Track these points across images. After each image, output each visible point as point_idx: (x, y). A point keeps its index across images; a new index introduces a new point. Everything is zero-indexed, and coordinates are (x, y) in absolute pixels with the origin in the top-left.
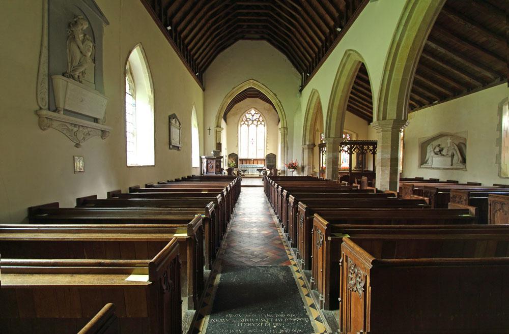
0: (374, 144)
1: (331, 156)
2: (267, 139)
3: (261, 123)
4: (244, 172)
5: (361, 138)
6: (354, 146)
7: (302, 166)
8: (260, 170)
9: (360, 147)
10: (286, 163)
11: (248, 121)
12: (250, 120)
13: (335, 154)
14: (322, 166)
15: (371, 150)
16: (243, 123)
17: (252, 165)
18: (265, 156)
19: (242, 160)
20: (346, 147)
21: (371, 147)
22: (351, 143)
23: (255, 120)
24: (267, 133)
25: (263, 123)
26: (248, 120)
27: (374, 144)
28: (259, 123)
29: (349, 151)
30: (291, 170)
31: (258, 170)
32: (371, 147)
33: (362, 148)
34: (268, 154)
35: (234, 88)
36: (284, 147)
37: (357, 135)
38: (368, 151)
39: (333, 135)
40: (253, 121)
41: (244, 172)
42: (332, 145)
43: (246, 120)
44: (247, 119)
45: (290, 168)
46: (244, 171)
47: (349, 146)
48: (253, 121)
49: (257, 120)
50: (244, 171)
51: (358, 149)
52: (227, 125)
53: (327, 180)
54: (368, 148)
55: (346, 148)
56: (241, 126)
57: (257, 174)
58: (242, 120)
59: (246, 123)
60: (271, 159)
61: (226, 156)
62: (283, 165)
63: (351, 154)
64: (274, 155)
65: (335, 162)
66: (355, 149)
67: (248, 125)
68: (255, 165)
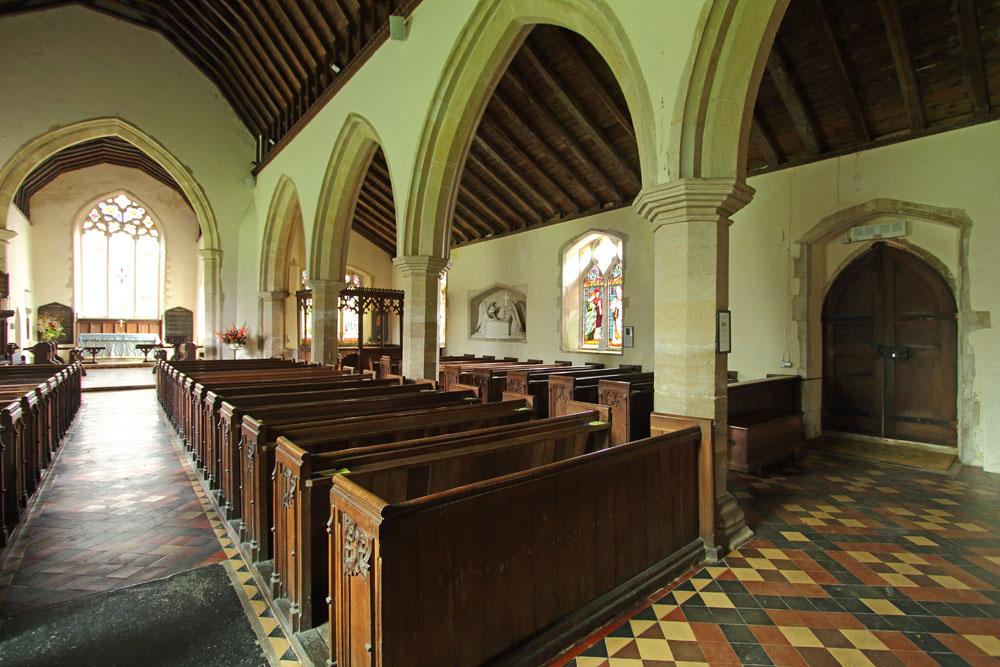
0: (400, 296)
1: (323, 317)
2: (166, 274)
3: (148, 233)
4: (94, 353)
5: (380, 285)
6: (367, 298)
7: (258, 336)
8: (145, 348)
9: (378, 301)
10: (218, 330)
11: (106, 223)
12: (115, 220)
13: (330, 313)
14: (303, 337)
15: (396, 308)
16: (88, 225)
17: (119, 335)
18: (162, 313)
19: (87, 323)
20: (353, 300)
21: (396, 303)
22: (360, 292)
23: (130, 222)
24: (167, 259)
25: (154, 232)
26: (107, 219)
27: (400, 296)
28: (142, 231)
29: (357, 308)
30: (232, 346)
31: (138, 347)
32: (396, 303)
33: (382, 303)
34: (168, 308)
35: (58, 127)
36: (214, 294)
37: (373, 280)
38: (392, 308)
39: (325, 274)
40: (122, 224)
41: (94, 353)
42: (323, 296)
43: (101, 220)
44: (103, 216)
45: (228, 341)
46: (94, 351)
47: (357, 298)
48: (122, 224)
49: (138, 223)
50: (94, 351)
51: (375, 304)
52: (31, 224)
53: (314, 366)
54: (392, 303)
55: (351, 302)
56: (83, 231)
57: (138, 356)
58: (88, 219)
59: (101, 226)
60: (178, 323)
61: (28, 311)
62: (210, 335)
63: (361, 313)
64: (186, 311)
65: (329, 329)
66: (368, 304)
67: (108, 234)
68: (131, 335)
